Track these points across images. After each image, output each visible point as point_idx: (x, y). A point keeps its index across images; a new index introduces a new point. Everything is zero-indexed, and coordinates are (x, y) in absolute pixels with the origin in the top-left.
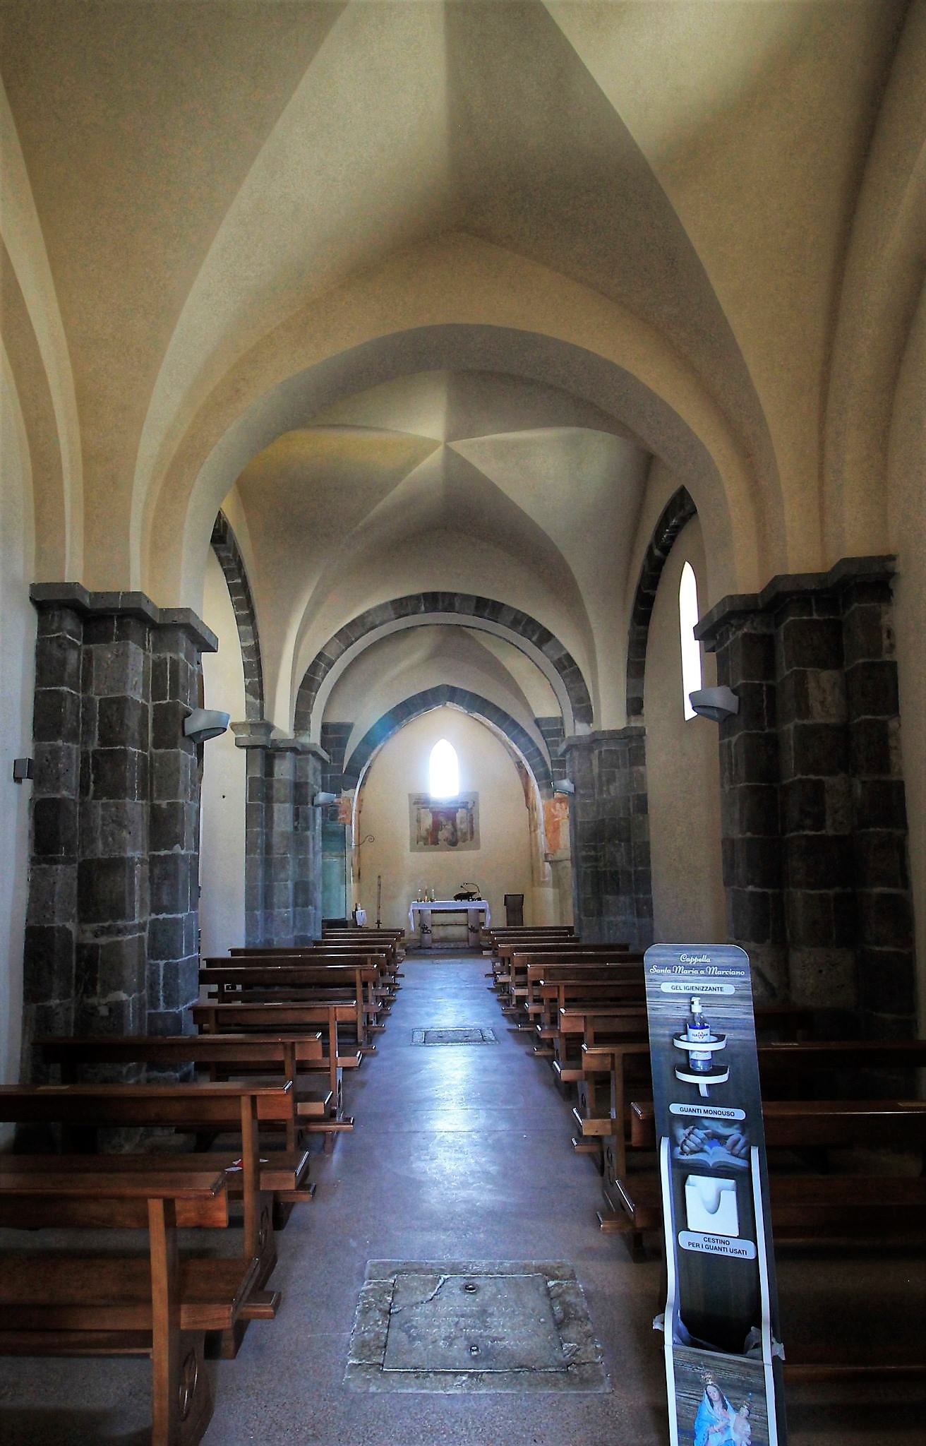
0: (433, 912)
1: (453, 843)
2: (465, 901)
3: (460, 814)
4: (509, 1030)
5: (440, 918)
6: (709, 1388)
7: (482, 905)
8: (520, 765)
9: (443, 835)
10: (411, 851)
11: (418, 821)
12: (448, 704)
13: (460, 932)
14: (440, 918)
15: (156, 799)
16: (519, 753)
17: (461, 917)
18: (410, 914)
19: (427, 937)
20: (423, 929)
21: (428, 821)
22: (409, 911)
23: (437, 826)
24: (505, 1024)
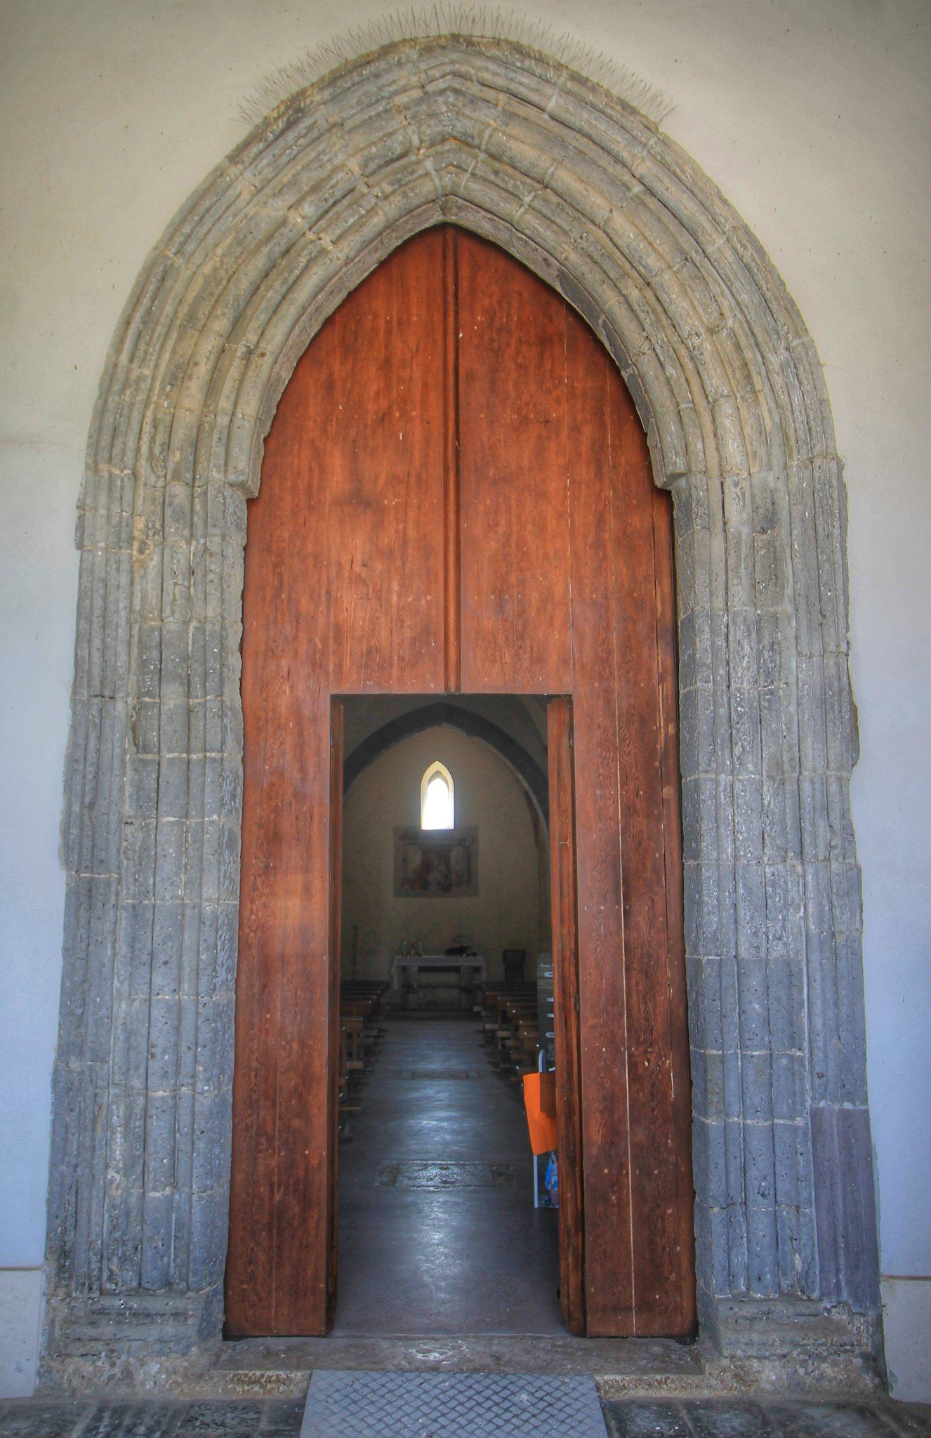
0: (422, 969)
1: (446, 888)
2: (457, 957)
3: (456, 853)
4: (492, 1072)
5: (426, 978)
6: (293, 307)
7: (478, 961)
8: (526, 793)
9: (434, 877)
10: (336, 700)
11: (405, 860)
12: (444, 724)
13: (452, 994)
14: (426, 978)
15: (152, 1190)
16: (526, 784)
17: (452, 978)
18: (394, 970)
19: (412, 997)
20: (408, 987)
21: (416, 860)
22: (391, 967)
23: (427, 866)
24: (490, 1068)
